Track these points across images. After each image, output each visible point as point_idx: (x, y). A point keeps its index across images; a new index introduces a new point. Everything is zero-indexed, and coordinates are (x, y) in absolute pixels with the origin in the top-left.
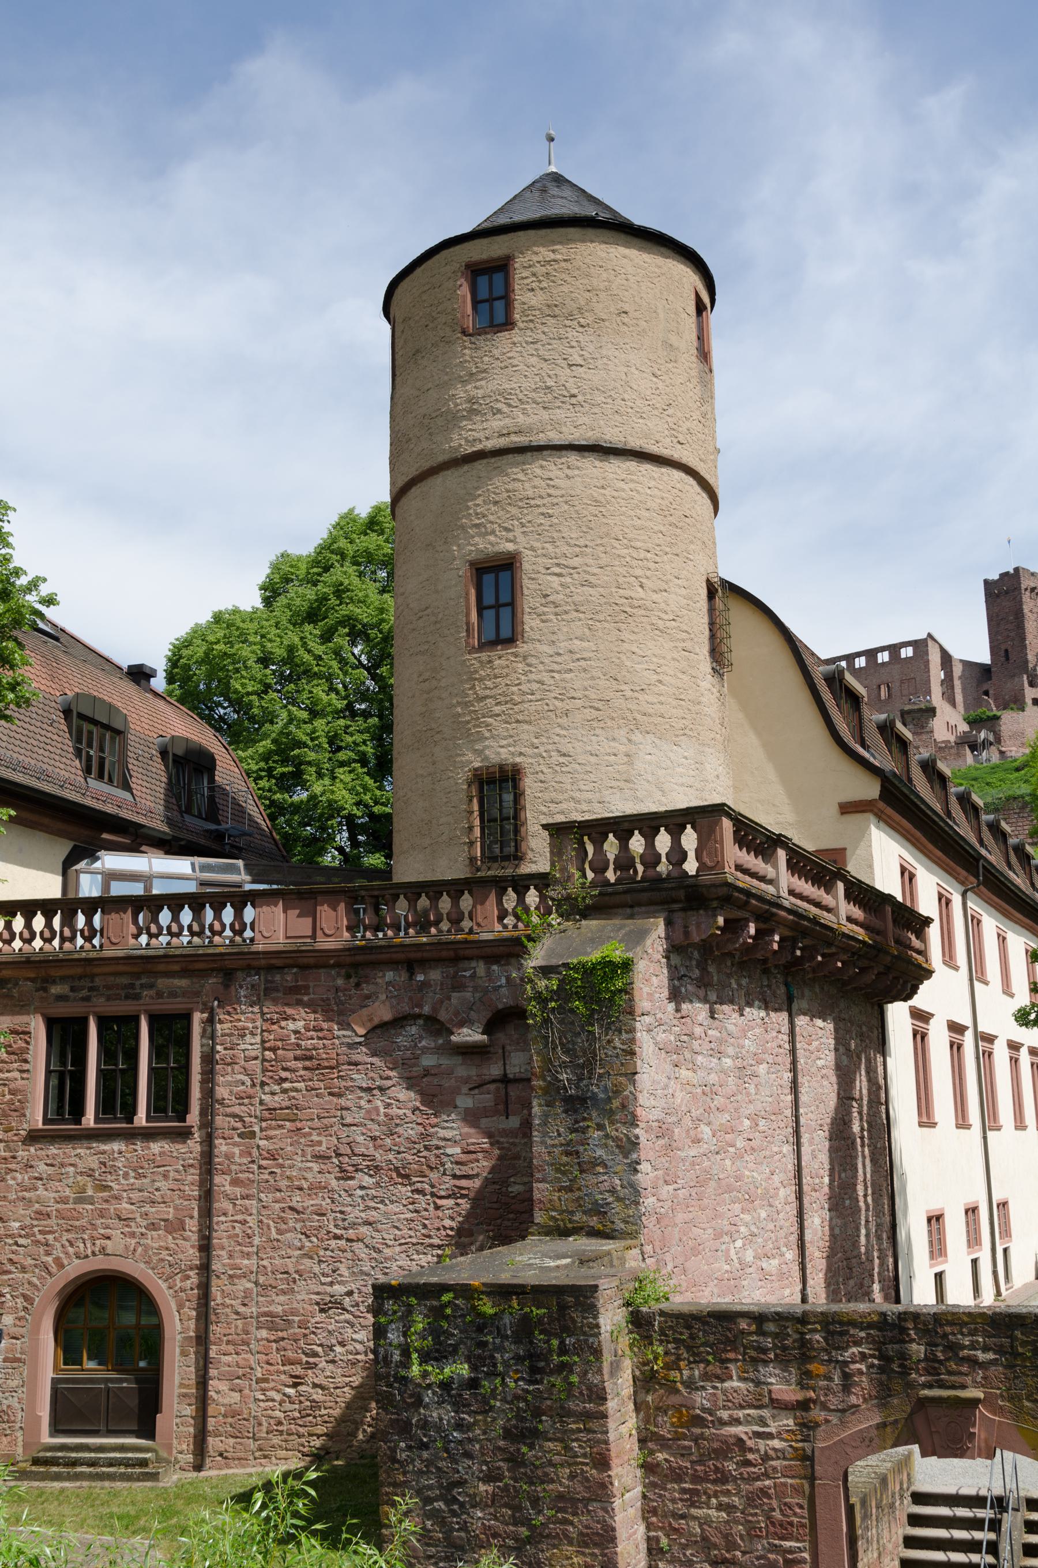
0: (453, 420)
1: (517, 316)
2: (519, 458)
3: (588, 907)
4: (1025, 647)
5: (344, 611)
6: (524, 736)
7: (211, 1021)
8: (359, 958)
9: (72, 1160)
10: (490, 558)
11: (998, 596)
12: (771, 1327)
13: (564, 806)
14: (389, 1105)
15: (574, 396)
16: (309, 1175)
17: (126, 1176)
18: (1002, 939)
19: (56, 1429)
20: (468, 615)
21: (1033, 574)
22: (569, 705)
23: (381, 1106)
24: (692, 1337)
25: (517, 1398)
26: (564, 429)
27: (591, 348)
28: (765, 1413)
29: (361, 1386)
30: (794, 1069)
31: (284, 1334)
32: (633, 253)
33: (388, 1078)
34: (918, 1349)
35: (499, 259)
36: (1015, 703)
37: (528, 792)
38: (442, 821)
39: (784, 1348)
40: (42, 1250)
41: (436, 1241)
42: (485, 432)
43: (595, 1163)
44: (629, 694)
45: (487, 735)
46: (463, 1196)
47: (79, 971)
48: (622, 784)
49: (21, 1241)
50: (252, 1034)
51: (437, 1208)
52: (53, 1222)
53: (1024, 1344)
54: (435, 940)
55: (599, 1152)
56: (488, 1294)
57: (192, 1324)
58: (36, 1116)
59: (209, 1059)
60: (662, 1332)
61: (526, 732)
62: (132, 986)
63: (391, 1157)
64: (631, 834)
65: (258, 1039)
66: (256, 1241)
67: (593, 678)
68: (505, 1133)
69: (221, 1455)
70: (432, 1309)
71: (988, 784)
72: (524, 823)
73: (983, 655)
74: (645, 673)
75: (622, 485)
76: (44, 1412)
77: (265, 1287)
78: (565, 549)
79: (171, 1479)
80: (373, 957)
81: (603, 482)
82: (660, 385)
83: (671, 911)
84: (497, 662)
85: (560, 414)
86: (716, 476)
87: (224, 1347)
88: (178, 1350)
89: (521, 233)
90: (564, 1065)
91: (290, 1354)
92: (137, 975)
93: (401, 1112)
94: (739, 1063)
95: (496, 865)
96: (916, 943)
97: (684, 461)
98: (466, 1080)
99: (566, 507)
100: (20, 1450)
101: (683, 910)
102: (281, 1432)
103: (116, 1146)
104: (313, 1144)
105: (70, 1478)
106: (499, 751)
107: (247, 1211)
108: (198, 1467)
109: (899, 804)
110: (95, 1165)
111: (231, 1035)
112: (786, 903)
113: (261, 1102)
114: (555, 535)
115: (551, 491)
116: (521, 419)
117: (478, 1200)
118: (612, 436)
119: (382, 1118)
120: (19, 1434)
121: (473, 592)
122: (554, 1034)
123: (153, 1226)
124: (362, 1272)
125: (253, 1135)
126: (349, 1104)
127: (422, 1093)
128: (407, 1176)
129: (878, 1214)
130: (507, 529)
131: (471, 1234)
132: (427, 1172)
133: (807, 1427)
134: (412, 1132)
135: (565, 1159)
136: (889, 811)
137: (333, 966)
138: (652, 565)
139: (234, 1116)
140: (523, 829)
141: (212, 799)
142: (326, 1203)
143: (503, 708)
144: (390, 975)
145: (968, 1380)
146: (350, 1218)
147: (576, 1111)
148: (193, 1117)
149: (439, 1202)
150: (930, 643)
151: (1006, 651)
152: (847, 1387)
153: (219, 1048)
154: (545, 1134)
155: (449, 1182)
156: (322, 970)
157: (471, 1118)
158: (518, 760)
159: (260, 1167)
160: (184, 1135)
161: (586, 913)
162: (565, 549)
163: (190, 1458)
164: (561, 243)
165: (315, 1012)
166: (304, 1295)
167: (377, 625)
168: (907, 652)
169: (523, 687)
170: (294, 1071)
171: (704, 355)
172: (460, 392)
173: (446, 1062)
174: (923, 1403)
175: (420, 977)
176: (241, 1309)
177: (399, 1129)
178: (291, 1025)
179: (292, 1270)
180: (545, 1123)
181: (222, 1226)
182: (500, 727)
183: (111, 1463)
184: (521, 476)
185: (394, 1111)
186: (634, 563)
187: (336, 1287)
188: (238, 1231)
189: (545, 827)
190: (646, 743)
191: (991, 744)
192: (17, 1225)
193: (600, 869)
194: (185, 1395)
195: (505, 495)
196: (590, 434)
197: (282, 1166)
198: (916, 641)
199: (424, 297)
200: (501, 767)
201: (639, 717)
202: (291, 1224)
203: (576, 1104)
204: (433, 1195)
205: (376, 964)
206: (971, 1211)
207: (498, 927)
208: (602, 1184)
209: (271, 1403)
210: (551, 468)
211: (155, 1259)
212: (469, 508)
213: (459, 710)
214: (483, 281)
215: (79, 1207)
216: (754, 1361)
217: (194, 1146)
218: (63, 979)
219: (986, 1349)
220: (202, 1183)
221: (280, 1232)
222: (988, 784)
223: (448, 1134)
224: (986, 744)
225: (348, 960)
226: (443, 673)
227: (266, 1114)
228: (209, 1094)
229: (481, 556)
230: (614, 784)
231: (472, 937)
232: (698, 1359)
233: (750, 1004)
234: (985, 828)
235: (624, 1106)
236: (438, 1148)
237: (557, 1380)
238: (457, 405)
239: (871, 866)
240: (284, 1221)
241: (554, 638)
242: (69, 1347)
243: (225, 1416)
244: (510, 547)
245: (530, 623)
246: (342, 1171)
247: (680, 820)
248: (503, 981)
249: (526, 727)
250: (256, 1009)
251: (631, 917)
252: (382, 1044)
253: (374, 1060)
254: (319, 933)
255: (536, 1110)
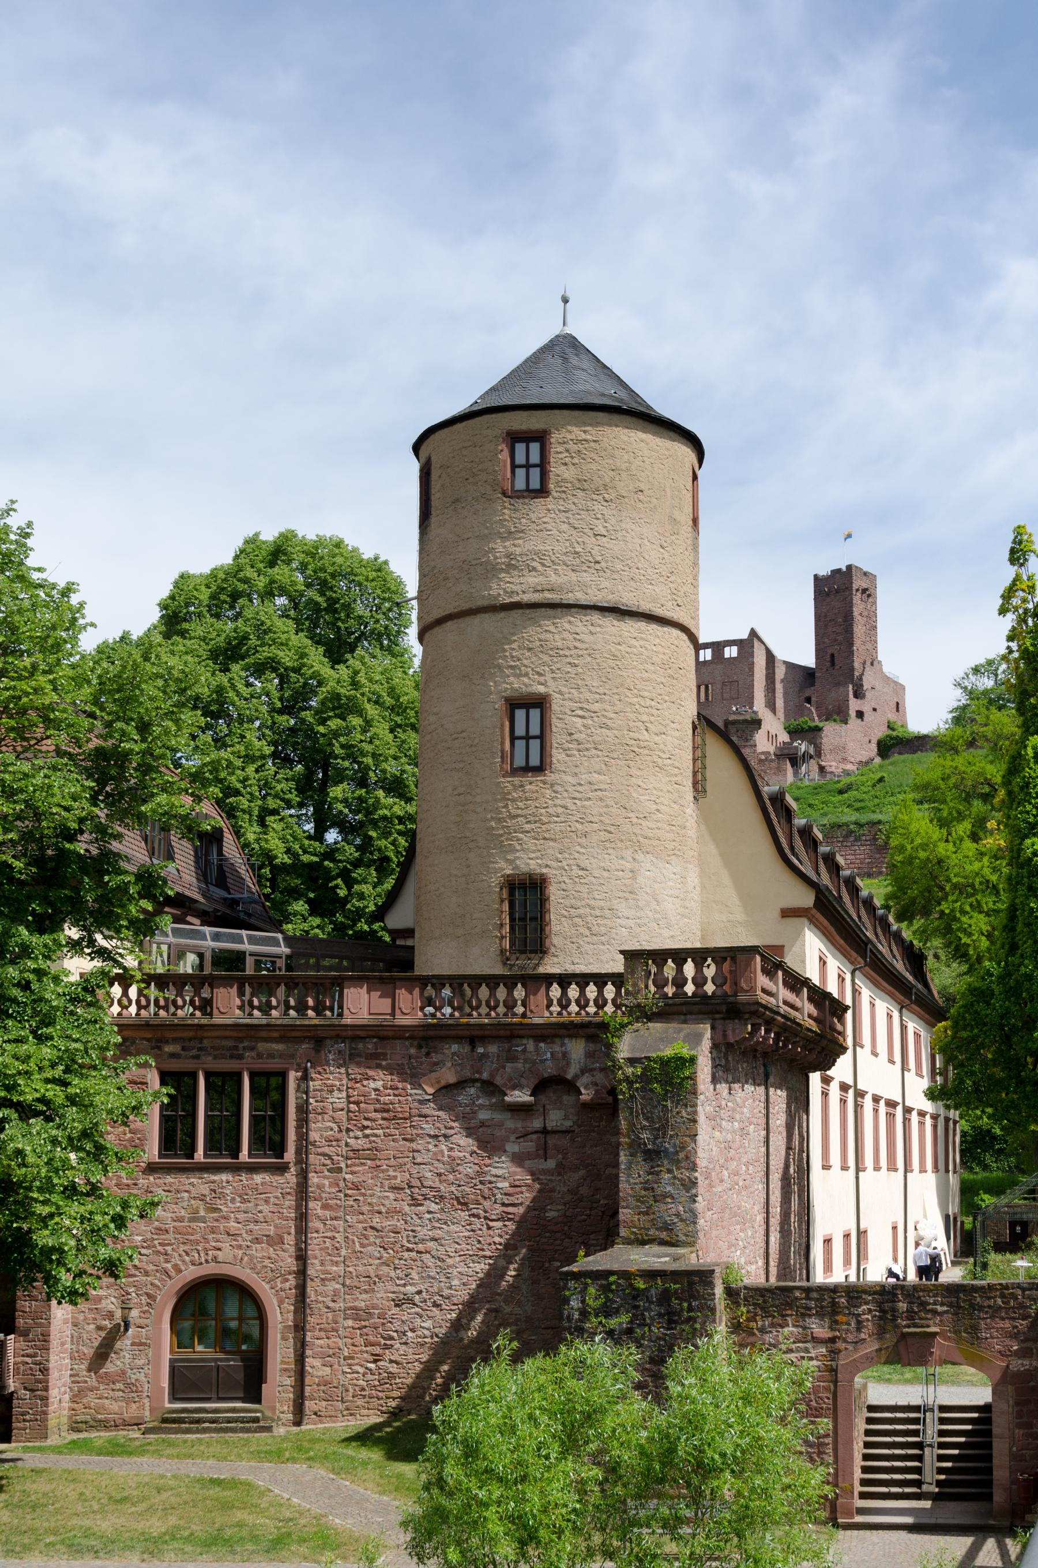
0: (491, 571)
1: (551, 486)
2: (550, 612)
3: (654, 1014)
4: (852, 653)
5: (265, 653)
6: (550, 851)
7: (305, 1077)
8: (431, 1033)
9: (187, 1188)
10: (522, 697)
11: (828, 594)
12: (815, 1295)
13: (581, 911)
14: (452, 1149)
15: (598, 562)
16: (387, 1202)
17: (233, 1200)
18: (873, 1005)
19: (174, 1397)
20: (503, 743)
21: (865, 574)
22: (588, 827)
23: (445, 1148)
24: (765, 1302)
25: (659, 1338)
26: (589, 591)
27: (613, 521)
28: (809, 1345)
29: (428, 1361)
30: (767, 1129)
31: (366, 1323)
32: (648, 437)
33: (451, 1128)
34: (902, 1306)
35: (537, 431)
36: (838, 714)
37: (552, 898)
38: (475, 916)
39: (822, 1307)
40: (162, 1258)
41: (488, 1253)
42: (522, 586)
43: (665, 1196)
44: (635, 820)
45: (518, 848)
46: (509, 1220)
47: (191, 1034)
48: (627, 895)
49: (143, 1251)
50: (339, 1090)
51: (489, 1228)
52: (171, 1236)
53: (964, 1301)
54: (495, 1021)
55: (669, 1188)
56: (641, 1276)
57: (291, 1316)
58: (152, 1151)
59: (303, 1110)
60: (746, 1299)
61: (552, 849)
62: (236, 1048)
63: (453, 1189)
64: (685, 961)
65: (344, 1094)
66: (343, 1252)
67: (607, 806)
68: (544, 1172)
69: (315, 1414)
70: (601, 1286)
71: (810, 805)
72: (549, 923)
73: (807, 658)
74: (647, 803)
75: (633, 642)
76: (165, 1384)
77: (351, 1288)
78: (588, 695)
79: (280, 1431)
80: (442, 1033)
81: (619, 639)
82: (666, 555)
83: (714, 1019)
84: (528, 787)
85: (586, 577)
86: (697, 624)
87: (317, 1333)
88: (279, 1336)
89: (557, 412)
90: (643, 1128)
91: (371, 1338)
92: (240, 1039)
93: (461, 1155)
94: (742, 1125)
95: (523, 956)
96: (839, 1027)
97: (681, 621)
98: (514, 1131)
99: (589, 659)
100: (147, 1413)
101: (724, 1019)
102: (364, 1396)
103: (224, 1177)
104: (389, 1178)
105: (198, 1431)
106: (529, 863)
107: (335, 1229)
108: (298, 1423)
109: (831, 915)
110: (206, 1192)
111: (321, 1090)
112: (782, 1011)
113: (347, 1145)
114: (580, 682)
115: (577, 644)
116: (553, 578)
117: (522, 1222)
118: (628, 599)
119: (446, 1159)
120: (146, 1401)
121: (507, 723)
122: (637, 1106)
123: (257, 1241)
124: (429, 1277)
125: (339, 1170)
126: (419, 1147)
127: (478, 1140)
128: (466, 1204)
129: (800, 1236)
130: (539, 674)
131: (515, 1248)
132: (482, 1201)
133: (834, 1353)
134: (471, 1170)
135: (643, 1193)
136: (818, 915)
137: (407, 1038)
138: (655, 712)
139: (324, 1155)
140: (547, 929)
141: (220, 867)
142: (400, 1224)
143: (533, 826)
144: (455, 1047)
145: (931, 1322)
146: (420, 1235)
147: (652, 1160)
148: (290, 1155)
149: (491, 1224)
150: (756, 643)
151: (832, 656)
152: (859, 1329)
153: (311, 1100)
154: (629, 1175)
155: (499, 1209)
156: (397, 1041)
157: (518, 1159)
158: (544, 871)
159: (346, 1195)
160: (283, 1169)
161: (651, 1017)
162: (588, 695)
163: (290, 1416)
164: (591, 425)
165: (391, 1074)
166: (383, 1294)
167: (297, 670)
168: (731, 652)
169: (549, 810)
170: (374, 1120)
171: (695, 521)
172: (500, 547)
173: (498, 1116)
174: (904, 1336)
175: (481, 1050)
176: (331, 1305)
177: (460, 1168)
178: (372, 1085)
179: (373, 1275)
180: (629, 1168)
181: (315, 1241)
182: (530, 843)
183: (229, 1421)
184: (552, 628)
185: (456, 1154)
186: (642, 710)
187: (408, 1287)
188: (328, 1244)
189: (622, 952)
190: (646, 861)
191: (811, 757)
192: (140, 1238)
193: (660, 984)
194: (285, 1370)
195: (538, 643)
196: (611, 597)
197: (364, 1195)
198: (741, 641)
199: (465, 452)
200: (530, 875)
201: (641, 839)
202: (372, 1239)
203: (653, 1155)
204: (486, 1218)
205: (443, 1038)
206: (847, 1236)
207: (547, 1014)
208: (669, 1210)
209: (356, 1374)
210: (578, 624)
211: (259, 1266)
212: (505, 651)
213: (493, 824)
214: (520, 448)
215: (194, 1225)
216: (803, 1315)
217: (291, 1178)
218: (175, 1040)
219: (942, 1304)
220: (298, 1207)
221: (362, 1245)
222: (810, 805)
223: (499, 1172)
224: (806, 757)
225: (421, 1034)
226: (478, 791)
227: (351, 1154)
228: (303, 1138)
229: (516, 694)
230: (621, 894)
231: (526, 1021)
232: (767, 1314)
233: (747, 1082)
234: (842, 884)
235: (687, 1157)
236: (490, 1182)
237: (686, 1327)
238: (496, 558)
239: (803, 962)
240: (366, 1237)
241: (577, 770)
242: (181, 1339)
243: (318, 1385)
244: (542, 689)
245: (557, 756)
246: (413, 1199)
247: (724, 955)
248: (549, 1055)
249: (552, 844)
250: (343, 1070)
251: (685, 1022)
252: (446, 1101)
253: (440, 1113)
254: (397, 1011)
255: (623, 1158)
